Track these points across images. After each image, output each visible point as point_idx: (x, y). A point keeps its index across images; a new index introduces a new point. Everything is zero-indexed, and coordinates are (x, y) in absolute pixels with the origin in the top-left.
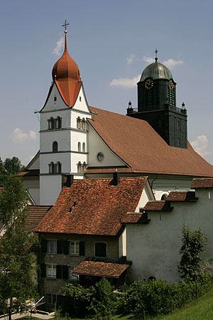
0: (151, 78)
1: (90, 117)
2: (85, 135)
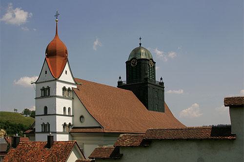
1: (75, 87)
2: (71, 101)
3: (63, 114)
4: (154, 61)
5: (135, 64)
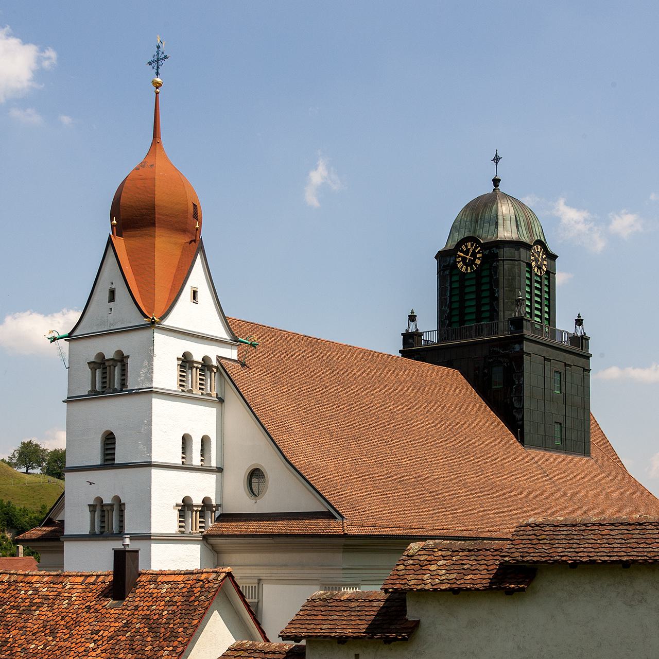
0: (473, 239)
3: (178, 461)
4: (552, 249)
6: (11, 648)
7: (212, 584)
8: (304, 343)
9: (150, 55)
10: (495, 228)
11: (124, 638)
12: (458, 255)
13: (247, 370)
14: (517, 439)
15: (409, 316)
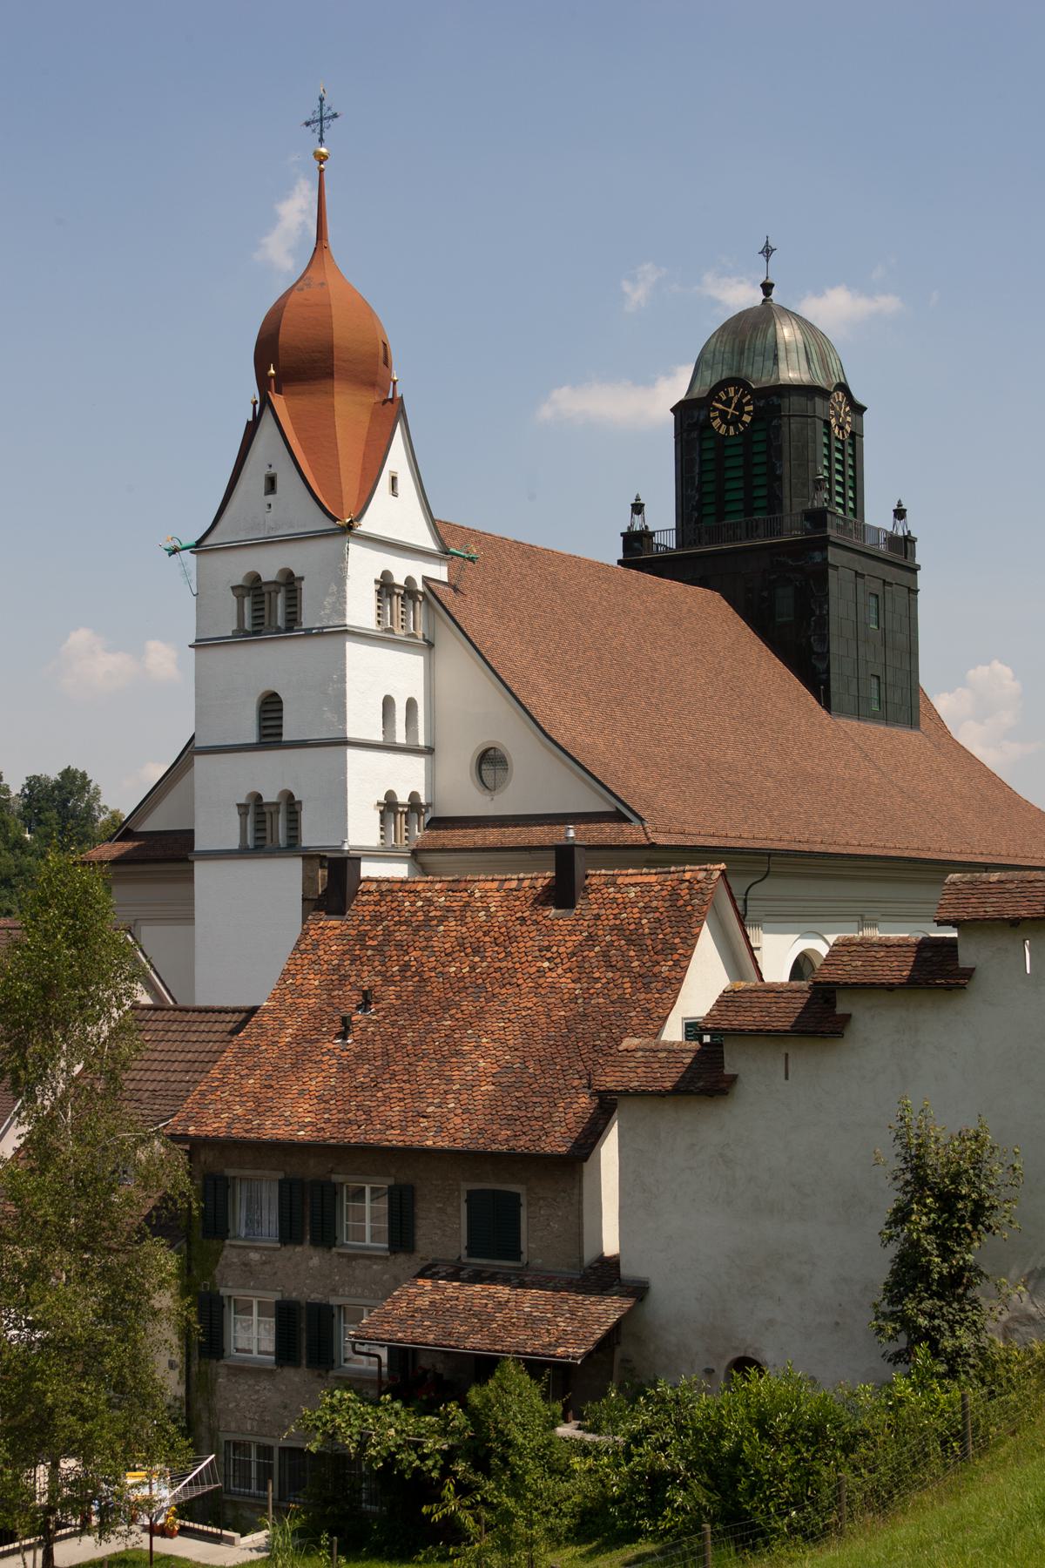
0: (739, 383)
1: (440, 572)
3: (378, 737)
4: (859, 397)
5: (736, 420)
6: (418, 973)
7: (703, 885)
8: (517, 553)
9: (309, 110)
10: (774, 364)
11: (592, 954)
12: (714, 406)
13: (461, 597)
14: (820, 702)
15: (632, 505)
